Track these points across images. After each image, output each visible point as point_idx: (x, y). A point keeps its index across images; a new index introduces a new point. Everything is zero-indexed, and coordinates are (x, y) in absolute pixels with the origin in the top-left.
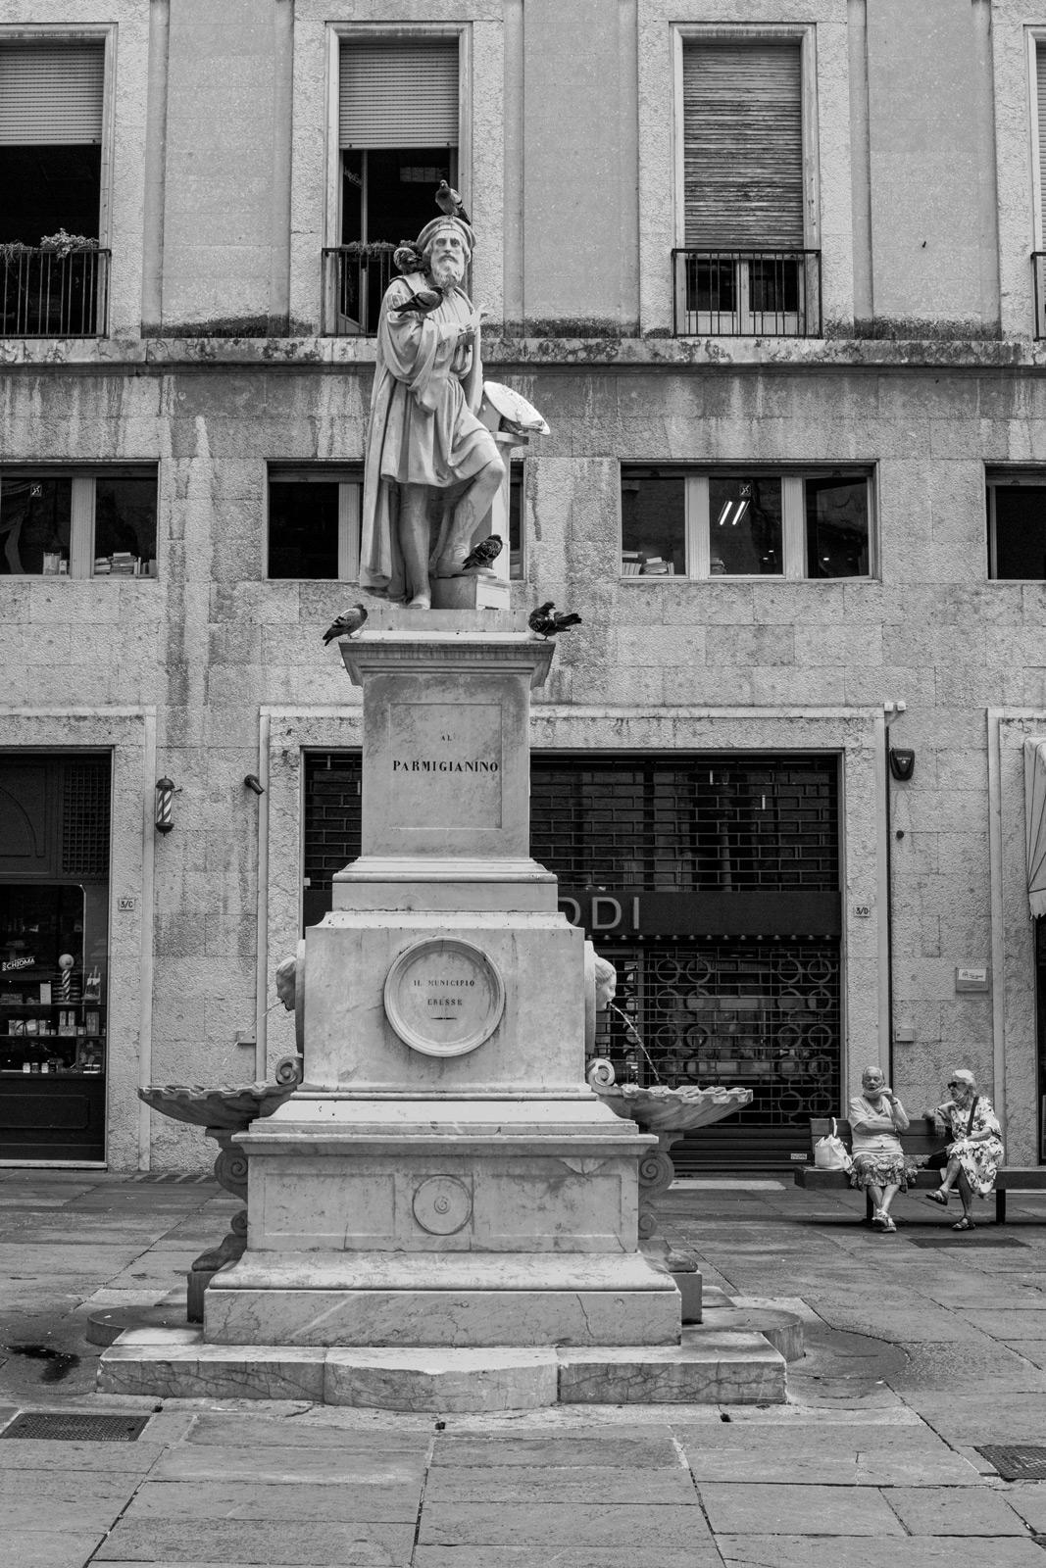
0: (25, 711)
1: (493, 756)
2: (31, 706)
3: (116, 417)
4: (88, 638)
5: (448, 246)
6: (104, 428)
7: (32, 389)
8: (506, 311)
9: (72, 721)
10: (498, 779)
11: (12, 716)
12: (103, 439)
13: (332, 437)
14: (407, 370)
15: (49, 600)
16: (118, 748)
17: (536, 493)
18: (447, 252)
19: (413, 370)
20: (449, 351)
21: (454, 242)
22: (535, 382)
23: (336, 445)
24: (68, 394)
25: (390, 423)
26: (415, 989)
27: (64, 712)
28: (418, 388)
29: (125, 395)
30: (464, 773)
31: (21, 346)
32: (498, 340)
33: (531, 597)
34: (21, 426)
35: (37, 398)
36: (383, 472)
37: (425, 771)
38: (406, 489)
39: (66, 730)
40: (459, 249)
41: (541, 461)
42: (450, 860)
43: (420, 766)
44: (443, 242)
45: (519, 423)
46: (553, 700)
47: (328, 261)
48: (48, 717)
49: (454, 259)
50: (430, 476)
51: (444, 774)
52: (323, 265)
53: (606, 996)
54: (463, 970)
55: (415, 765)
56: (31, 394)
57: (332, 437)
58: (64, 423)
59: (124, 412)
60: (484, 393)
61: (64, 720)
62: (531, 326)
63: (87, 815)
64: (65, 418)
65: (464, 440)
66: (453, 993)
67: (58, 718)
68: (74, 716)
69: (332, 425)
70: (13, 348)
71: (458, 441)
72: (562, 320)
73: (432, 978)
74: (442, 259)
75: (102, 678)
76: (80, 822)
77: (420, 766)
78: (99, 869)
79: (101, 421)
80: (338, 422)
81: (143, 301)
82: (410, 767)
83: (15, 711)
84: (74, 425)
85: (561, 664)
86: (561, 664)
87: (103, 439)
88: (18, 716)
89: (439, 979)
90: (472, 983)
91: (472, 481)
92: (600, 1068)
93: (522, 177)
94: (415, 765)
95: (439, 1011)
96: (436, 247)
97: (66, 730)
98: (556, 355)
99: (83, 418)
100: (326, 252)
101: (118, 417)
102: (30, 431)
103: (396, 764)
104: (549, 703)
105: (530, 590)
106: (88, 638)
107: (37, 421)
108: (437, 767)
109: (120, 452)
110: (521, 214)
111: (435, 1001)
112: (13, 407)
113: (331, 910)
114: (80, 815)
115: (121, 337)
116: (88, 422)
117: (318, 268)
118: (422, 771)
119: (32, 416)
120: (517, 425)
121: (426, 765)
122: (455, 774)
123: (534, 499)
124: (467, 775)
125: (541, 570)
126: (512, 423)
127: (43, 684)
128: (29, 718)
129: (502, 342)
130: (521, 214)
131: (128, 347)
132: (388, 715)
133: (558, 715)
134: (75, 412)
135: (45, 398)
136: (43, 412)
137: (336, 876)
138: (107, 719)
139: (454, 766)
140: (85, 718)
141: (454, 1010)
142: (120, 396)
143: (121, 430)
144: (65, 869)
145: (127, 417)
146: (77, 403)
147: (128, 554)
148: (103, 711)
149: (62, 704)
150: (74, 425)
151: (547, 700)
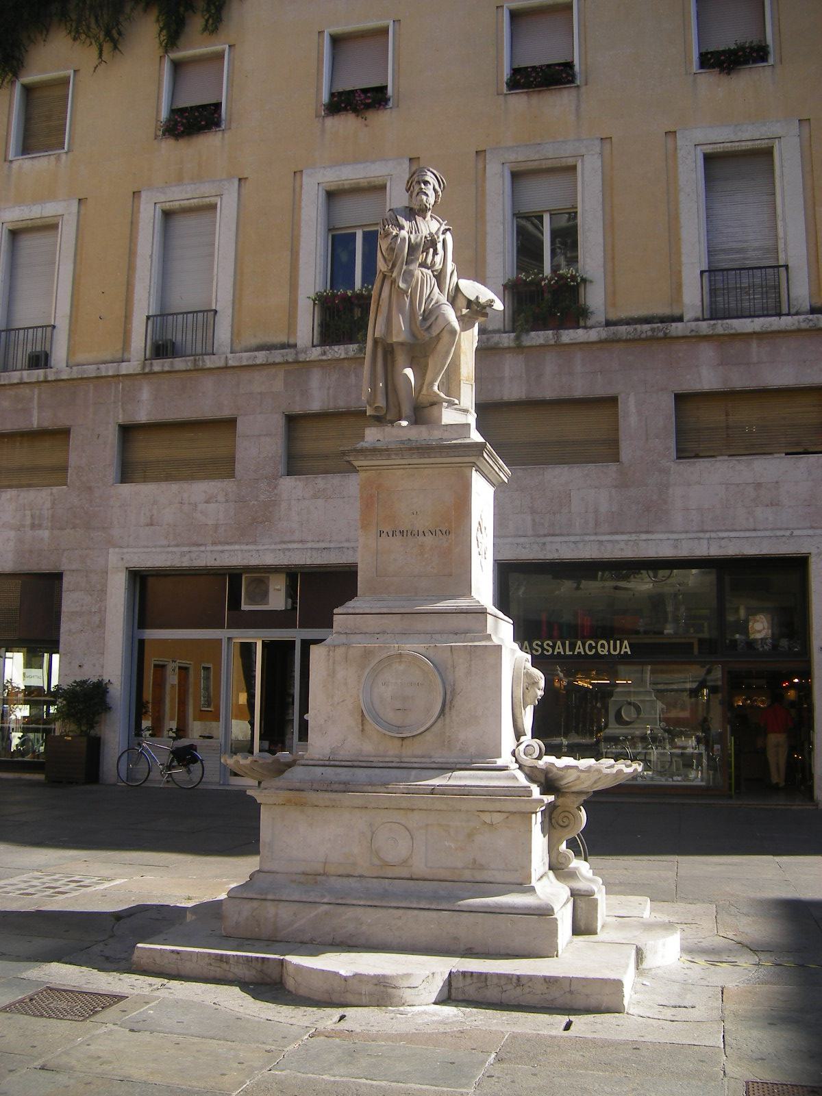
0: (346, 545)
1: (447, 524)
8: (606, 313)
11: (340, 548)
43: (398, 533)
70: (339, 349)
77: (398, 533)
82: (391, 534)
108: (409, 534)
121: (402, 533)
137: (336, 611)
139: (421, 533)
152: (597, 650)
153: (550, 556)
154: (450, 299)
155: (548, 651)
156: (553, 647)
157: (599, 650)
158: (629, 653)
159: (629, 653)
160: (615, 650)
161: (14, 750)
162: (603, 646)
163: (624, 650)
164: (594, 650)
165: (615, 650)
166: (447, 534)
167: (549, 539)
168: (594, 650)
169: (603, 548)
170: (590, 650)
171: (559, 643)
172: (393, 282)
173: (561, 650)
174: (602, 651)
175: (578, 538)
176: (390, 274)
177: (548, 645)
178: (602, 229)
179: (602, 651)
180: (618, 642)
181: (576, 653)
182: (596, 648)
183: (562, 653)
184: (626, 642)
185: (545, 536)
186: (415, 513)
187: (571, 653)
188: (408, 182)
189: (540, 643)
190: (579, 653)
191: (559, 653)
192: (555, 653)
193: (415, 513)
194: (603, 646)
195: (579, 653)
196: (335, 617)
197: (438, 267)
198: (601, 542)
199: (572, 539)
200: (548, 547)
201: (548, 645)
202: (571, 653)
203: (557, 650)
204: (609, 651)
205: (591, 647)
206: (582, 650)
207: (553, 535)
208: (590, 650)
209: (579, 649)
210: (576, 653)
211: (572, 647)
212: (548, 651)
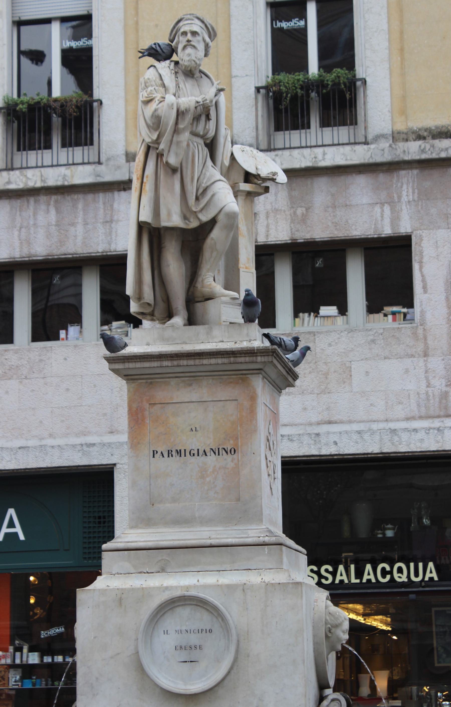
0: (50, 442)
1: (232, 442)
2: (55, 438)
3: (109, 222)
4: (95, 386)
5: (189, 36)
6: (101, 230)
7: (49, 205)
8: (393, 123)
9: (85, 448)
10: (236, 461)
11: (41, 446)
12: (100, 238)
13: (268, 226)
14: (155, 137)
15: (65, 359)
16: (118, 466)
17: (422, 258)
18: (188, 41)
19: (159, 137)
20: (189, 118)
21: (194, 33)
22: (417, 174)
23: (271, 232)
24: (75, 206)
25: (145, 180)
26: (164, 637)
27: (78, 441)
28: (163, 150)
29: (116, 205)
30: (209, 457)
31: (39, 174)
32: (388, 145)
33: (421, 336)
34: (41, 234)
35: (53, 212)
36: (140, 220)
37: (178, 457)
38: (162, 232)
39: (80, 454)
40: (199, 38)
41: (424, 234)
42: (199, 529)
43: (174, 453)
44: (185, 33)
45: (259, 175)
46: (442, 413)
47: (260, 97)
48: (66, 445)
49: (194, 47)
50: (176, 220)
51: (193, 459)
52: (256, 98)
53: (339, 639)
54: (203, 619)
55: (170, 453)
56: (48, 210)
57: (268, 226)
58: (72, 229)
59: (115, 218)
60: (232, 154)
61: (79, 448)
62: (413, 133)
63: (100, 518)
64: (73, 224)
65: (205, 190)
66: (194, 639)
67: (74, 446)
68: (86, 444)
69: (267, 217)
70: (33, 176)
71: (201, 191)
72: (437, 127)
73: (178, 628)
74: (185, 48)
75: (105, 414)
76: (95, 522)
77: (174, 453)
78: (94, 558)
79: (99, 225)
80: (272, 215)
81: (126, 136)
82: (166, 455)
83: (43, 442)
84: (80, 229)
85: (447, 386)
86: (447, 386)
87: (100, 238)
88: (45, 446)
89: (184, 628)
90: (210, 631)
91: (213, 222)
92: (333, 700)
93: (401, 22)
94: (170, 453)
95: (184, 656)
96: (181, 38)
97: (80, 454)
98: (432, 153)
99: (86, 224)
100: (258, 89)
101: (111, 221)
102: (48, 236)
103: (154, 453)
104: (439, 417)
105: (420, 331)
106: (95, 386)
107: (53, 229)
108: (188, 453)
109: (113, 247)
110: (402, 50)
111: (181, 647)
112: (35, 219)
113: (100, 574)
114: (95, 517)
115: (111, 163)
116: (90, 227)
117: (253, 102)
118: (176, 458)
119: (49, 225)
120: (257, 176)
121: (179, 452)
122: (202, 458)
123: (421, 262)
124: (211, 459)
125: (428, 316)
126: (254, 176)
127: (63, 421)
128: (53, 447)
129: (390, 146)
130: (402, 50)
131: (116, 170)
132: (147, 413)
133: (446, 425)
134: (80, 220)
135: (58, 211)
136: (57, 221)
137: (104, 546)
138: (110, 445)
139: (201, 452)
140: (94, 445)
141: (195, 654)
142: (112, 206)
143: (114, 230)
144: (85, 558)
145: (118, 221)
146: (81, 213)
147: (123, 322)
148: (108, 439)
149: (77, 435)
150: (80, 229)
151: (437, 414)
152: (392, 577)
153: (325, 451)
154: (225, 170)
155: (327, 579)
156: (334, 574)
157: (396, 575)
158: (436, 579)
159: (436, 579)
160: (417, 575)
161: (391, 627)
162: (400, 570)
163: (428, 575)
164: (388, 577)
165: (417, 575)
166: (233, 453)
167: (324, 429)
168: (388, 577)
169: (396, 438)
170: (384, 576)
171: (341, 568)
172: (160, 156)
173: (344, 578)
174: (400, 577)
175: (361, 427)
176: (156, 146)
177: (327, 571)
178: (385, 10)
179: (400, 577)
180: (421, 565)
181: (364, 581)
182: (391, 573)
183: (346, 581)
184: (431, 565)
185: (319, 424)
186: (194, 429)
187: (358, 581)
188: (172, 31)
189: (315, 569)
190: (369, 581)
191: (342, 581)
192: (337, 581)
193: (194, 429)
194: (400, 570)
195: (369, 581)
196: (105, 555)
197: (211, 134)
198: (394, 431)
199: (355, 427)
200: (323, 440)
201: (327, 571)
202: (358, 581)
203: (338, 578)
204: (409, 576)
205: (384, 573)
206: (372, 577)
207: (330, 422)
208: (384, 576)
209: (369, 574)
210: (364, 581)
211: (359, 574)
212: (327, 579)
